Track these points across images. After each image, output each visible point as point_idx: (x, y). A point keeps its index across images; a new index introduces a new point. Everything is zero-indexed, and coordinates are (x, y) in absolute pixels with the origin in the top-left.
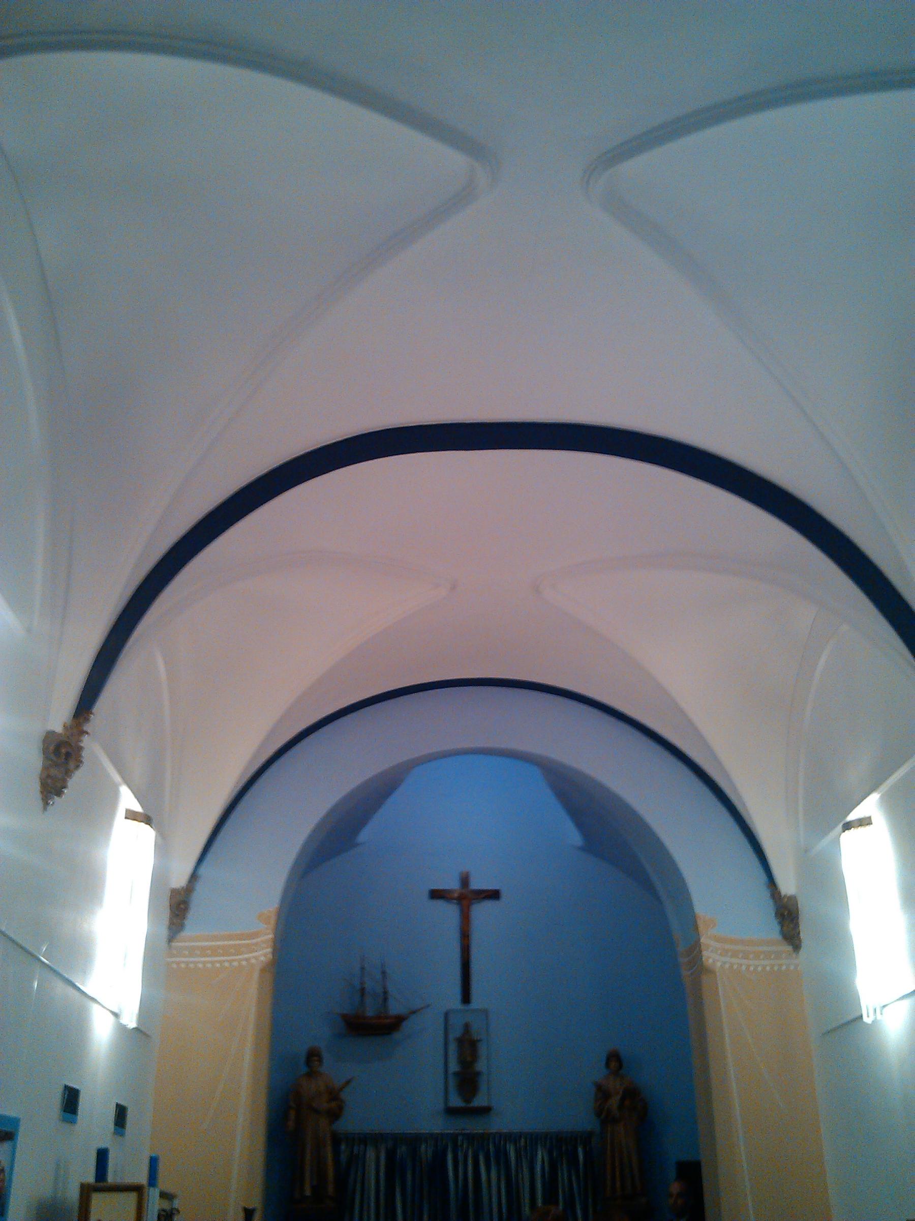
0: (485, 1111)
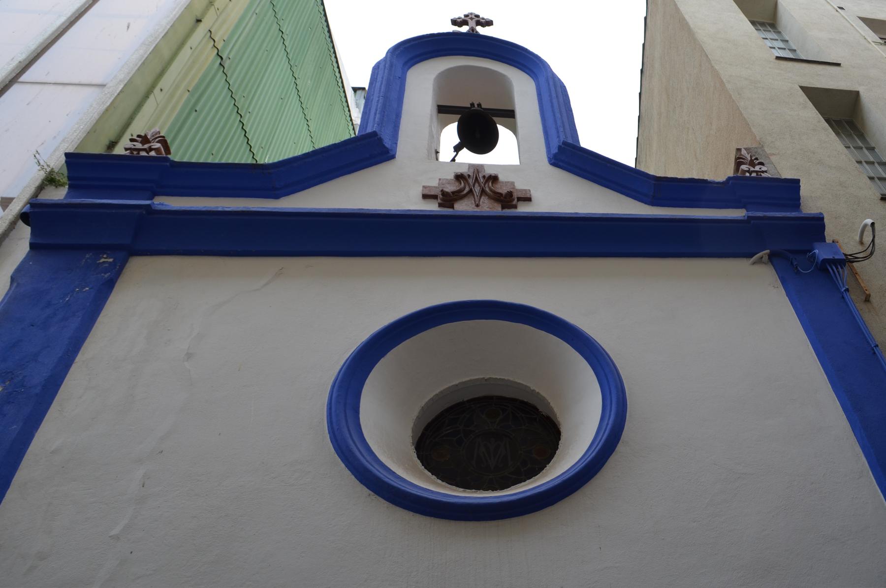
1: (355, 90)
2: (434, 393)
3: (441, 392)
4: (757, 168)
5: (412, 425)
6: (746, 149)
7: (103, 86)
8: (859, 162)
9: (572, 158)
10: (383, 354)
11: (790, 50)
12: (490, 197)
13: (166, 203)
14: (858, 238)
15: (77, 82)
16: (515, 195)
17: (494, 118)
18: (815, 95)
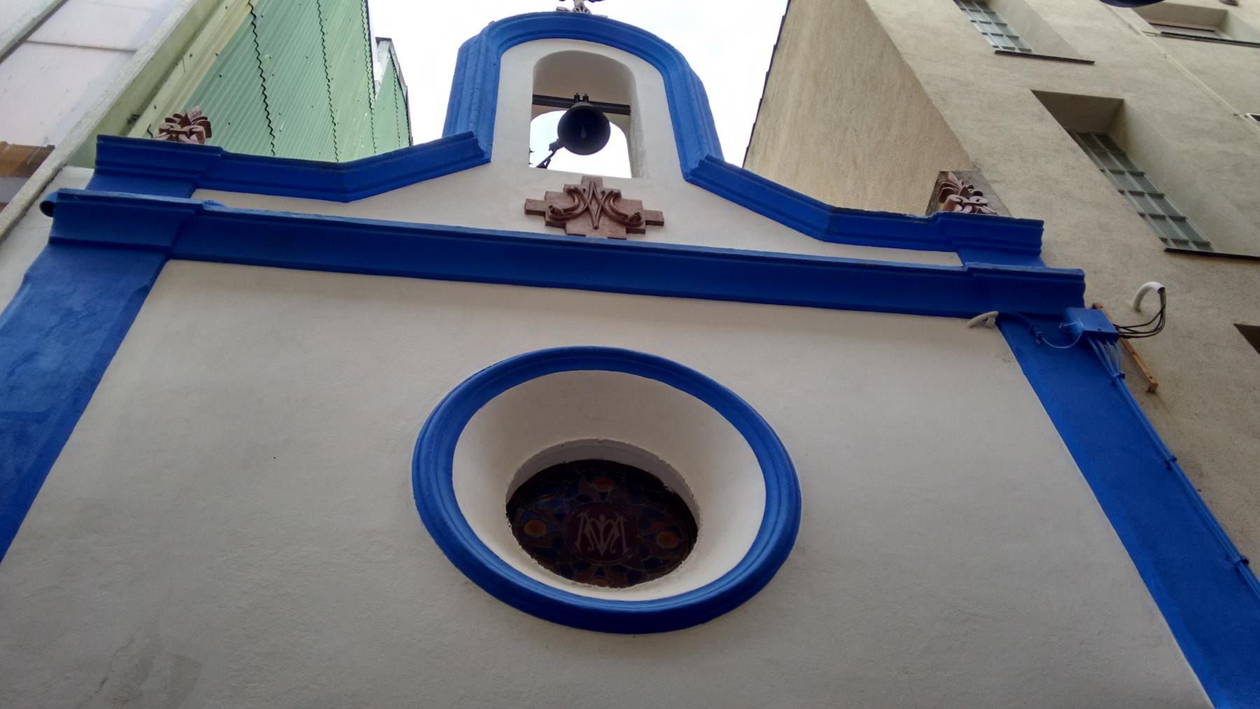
1: (379, 40)
4: (973, 200)
6: (955, 173)
7: (131, 52)
8: (1122, 192)
9: (709, 173)
10: (481, 405)
11: (1009, 37)
12: (611, 218)
13: (216, 200)
14: (1132, 303)
15: (99, 45)
16: (644, 218)
17: (607, 115)
18: (1058, 104)
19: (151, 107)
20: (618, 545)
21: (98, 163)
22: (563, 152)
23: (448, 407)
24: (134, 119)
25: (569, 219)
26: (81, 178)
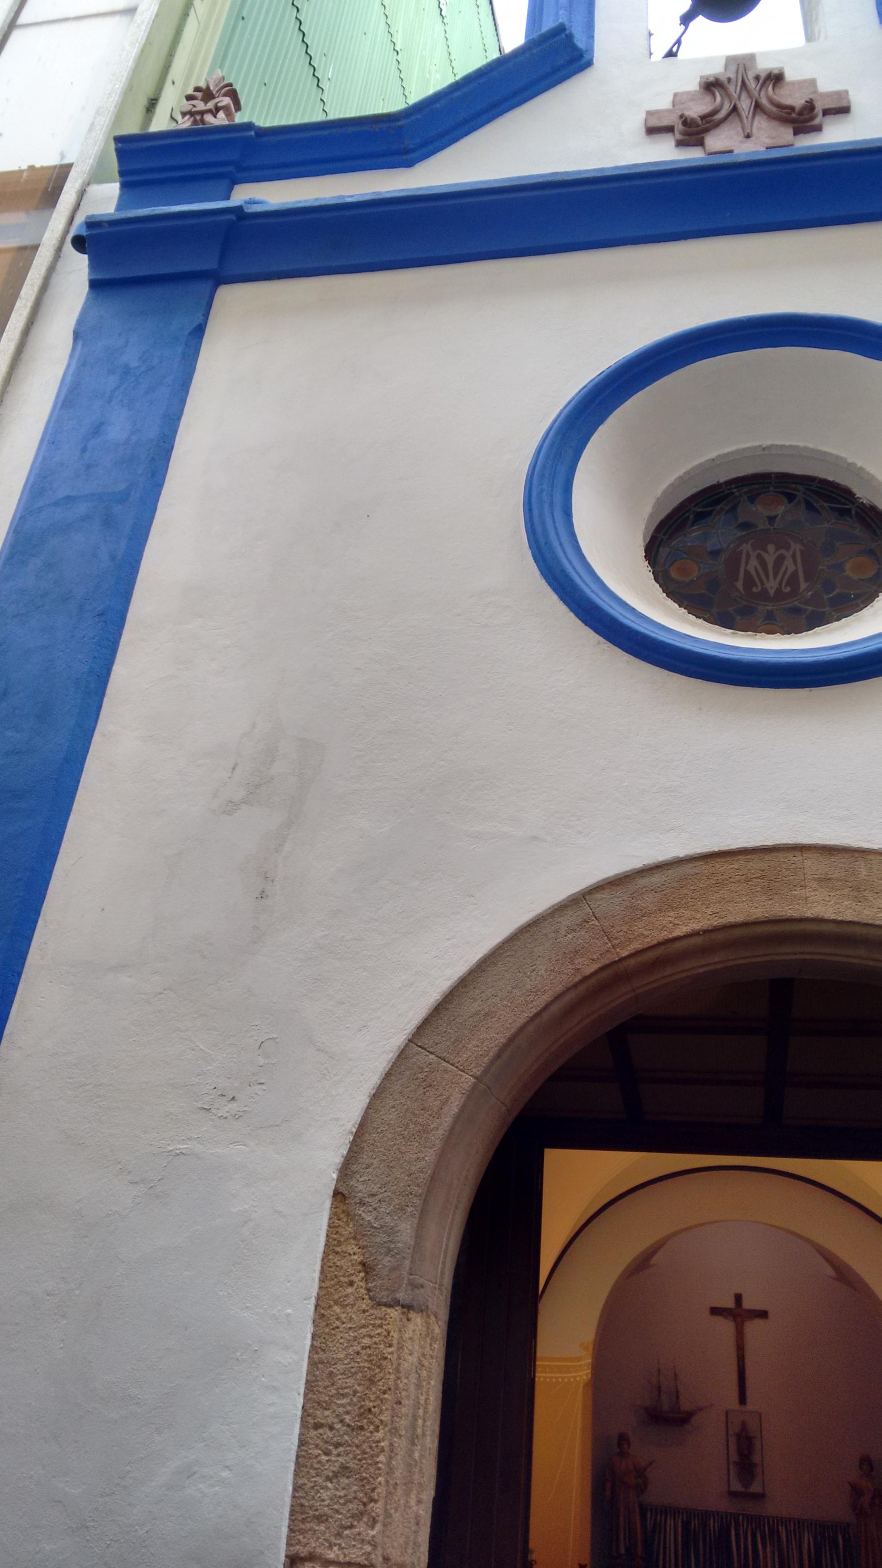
0: (761, 1496)
2: (676, 476)
3: (688, 473)
5: (643, 527)
7: (130, 11)
10: (601, 421)
12: (771, 116)
16: (819, 107)
19: (168, 86)
20: (793, 579)
21: (122, 173)
22: (701, 22)
23: (560, 428)
24: (152, 105)
25: (707, 130)
26: (106, 199)
